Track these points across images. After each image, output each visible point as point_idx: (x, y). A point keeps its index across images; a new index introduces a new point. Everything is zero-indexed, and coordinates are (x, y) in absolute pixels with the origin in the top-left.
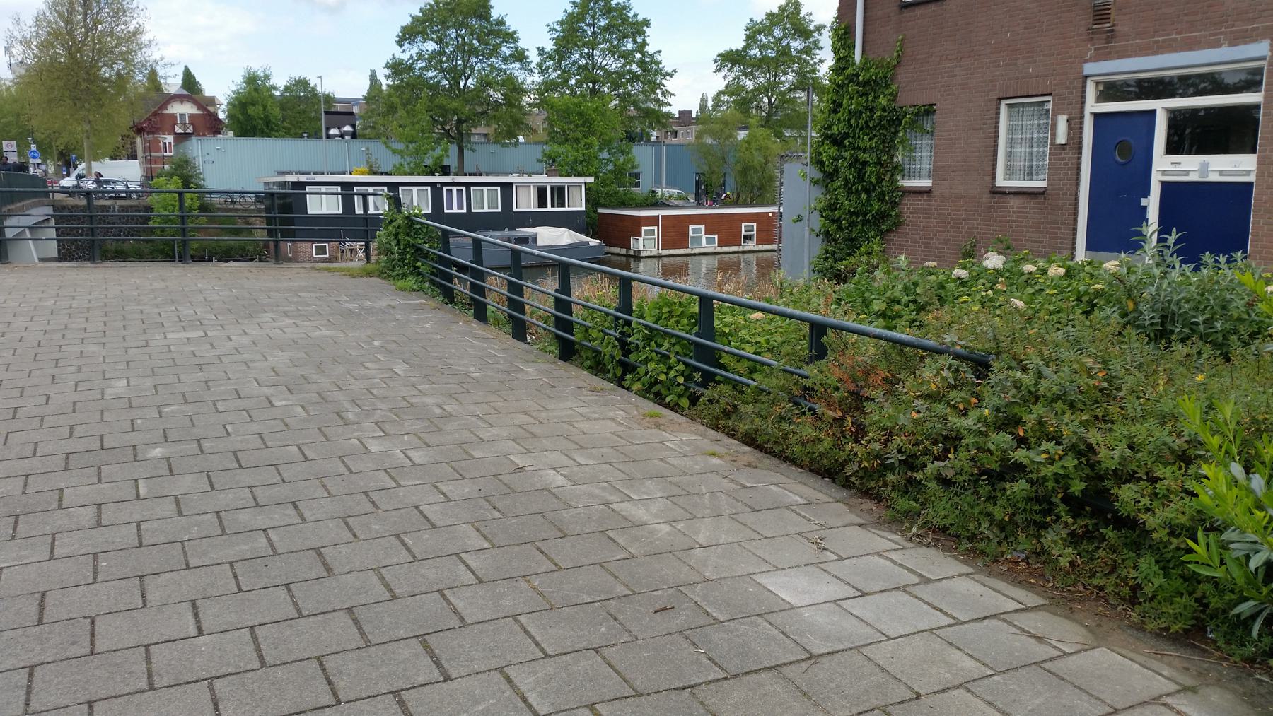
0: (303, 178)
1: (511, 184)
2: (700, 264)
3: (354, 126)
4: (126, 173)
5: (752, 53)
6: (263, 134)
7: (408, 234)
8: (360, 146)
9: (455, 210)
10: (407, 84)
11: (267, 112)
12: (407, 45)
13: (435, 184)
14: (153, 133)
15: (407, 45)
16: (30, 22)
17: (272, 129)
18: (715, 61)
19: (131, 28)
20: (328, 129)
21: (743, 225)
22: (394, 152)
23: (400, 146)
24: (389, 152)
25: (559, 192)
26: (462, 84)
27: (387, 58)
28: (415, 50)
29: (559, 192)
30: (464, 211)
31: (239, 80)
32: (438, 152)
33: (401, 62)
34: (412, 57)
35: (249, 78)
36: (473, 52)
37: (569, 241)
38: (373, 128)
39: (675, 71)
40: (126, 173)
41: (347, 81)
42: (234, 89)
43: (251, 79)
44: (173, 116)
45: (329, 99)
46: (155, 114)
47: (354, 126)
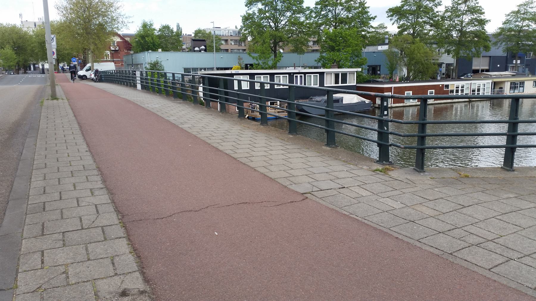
1: (323, 73)
2: (409, 111)
5: (405, 8)
18: (387, 12)
20: (194, 48)
21: (429, 91)
22: (253, 58)
24: (251, 58)
25: (344, 75)
29: (344, 75)
37: (357, 101)
39: (376, 17)
43: (145, 26)
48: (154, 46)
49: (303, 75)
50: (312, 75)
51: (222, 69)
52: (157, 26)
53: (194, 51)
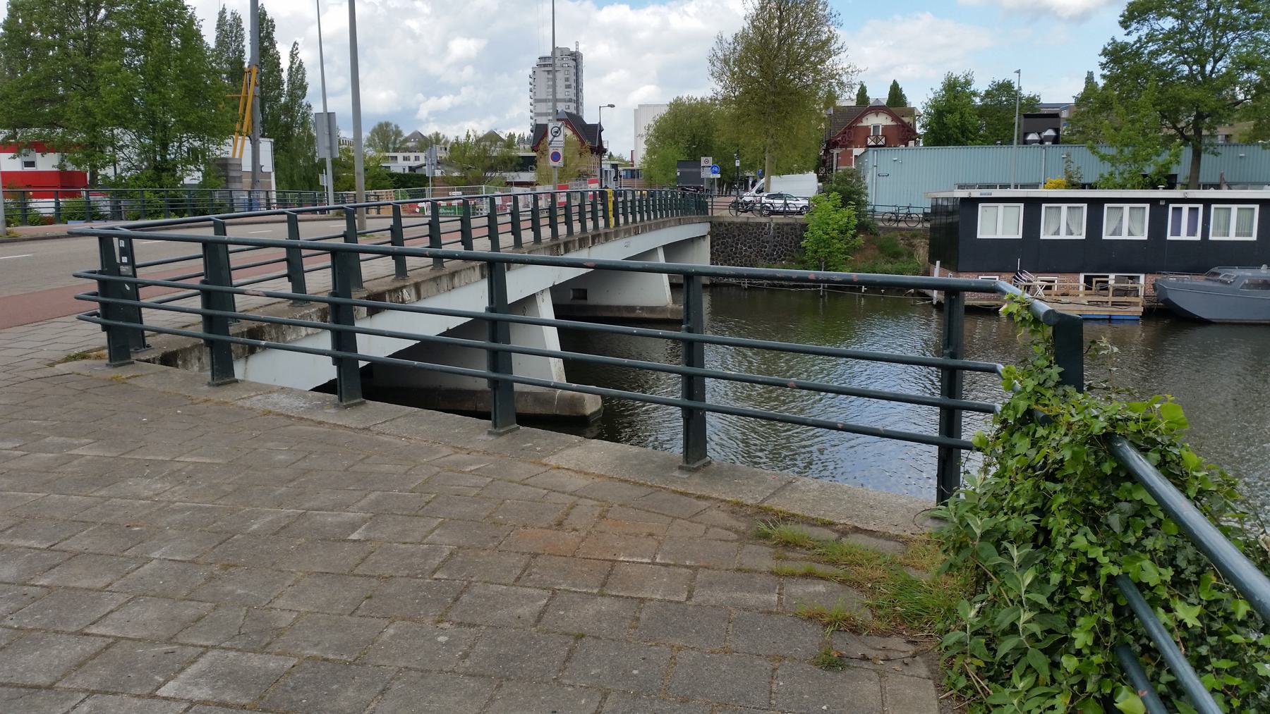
0: (976, 193)
3: (1057, 130)
4: (800, 188)
6: (958, 143)
7: (1092, 518)
8: (1060, 152)
9: (1184, 236)
10: (1130, 72)
11: (966, 119)
12: (1134, 25)
13: (1158, 200)
14: (846, 146)
15: (1134, 25)
16: (731, 40)
17: (968, 138)
19: (824, 37)
20: (1026, 134)
22: (1103, 158)
23: (1113, 151)
24: (1097, 159)
26: (1209, 68)
27: (1105, 41)
28: (1145, 30)
30: (1198, 237)
31: (938, 87)
32: (1166, 156)
33: (1125, 46)
34: (1140, 39)
35: (949, 85)
36: (1231, 25)
38: (1082, 133)
40: (800, 188)
41: (1058, 83)
42: (932, 96)
44: (867, 128)
45: (1033, 101)
46: (850, 127)
47: (1057, 130)
48: (963, 133)
49: (1201, 206)
50: (1234, 207)
51: (1023, 187)
52: (981, 85)
53: (1025, 142)
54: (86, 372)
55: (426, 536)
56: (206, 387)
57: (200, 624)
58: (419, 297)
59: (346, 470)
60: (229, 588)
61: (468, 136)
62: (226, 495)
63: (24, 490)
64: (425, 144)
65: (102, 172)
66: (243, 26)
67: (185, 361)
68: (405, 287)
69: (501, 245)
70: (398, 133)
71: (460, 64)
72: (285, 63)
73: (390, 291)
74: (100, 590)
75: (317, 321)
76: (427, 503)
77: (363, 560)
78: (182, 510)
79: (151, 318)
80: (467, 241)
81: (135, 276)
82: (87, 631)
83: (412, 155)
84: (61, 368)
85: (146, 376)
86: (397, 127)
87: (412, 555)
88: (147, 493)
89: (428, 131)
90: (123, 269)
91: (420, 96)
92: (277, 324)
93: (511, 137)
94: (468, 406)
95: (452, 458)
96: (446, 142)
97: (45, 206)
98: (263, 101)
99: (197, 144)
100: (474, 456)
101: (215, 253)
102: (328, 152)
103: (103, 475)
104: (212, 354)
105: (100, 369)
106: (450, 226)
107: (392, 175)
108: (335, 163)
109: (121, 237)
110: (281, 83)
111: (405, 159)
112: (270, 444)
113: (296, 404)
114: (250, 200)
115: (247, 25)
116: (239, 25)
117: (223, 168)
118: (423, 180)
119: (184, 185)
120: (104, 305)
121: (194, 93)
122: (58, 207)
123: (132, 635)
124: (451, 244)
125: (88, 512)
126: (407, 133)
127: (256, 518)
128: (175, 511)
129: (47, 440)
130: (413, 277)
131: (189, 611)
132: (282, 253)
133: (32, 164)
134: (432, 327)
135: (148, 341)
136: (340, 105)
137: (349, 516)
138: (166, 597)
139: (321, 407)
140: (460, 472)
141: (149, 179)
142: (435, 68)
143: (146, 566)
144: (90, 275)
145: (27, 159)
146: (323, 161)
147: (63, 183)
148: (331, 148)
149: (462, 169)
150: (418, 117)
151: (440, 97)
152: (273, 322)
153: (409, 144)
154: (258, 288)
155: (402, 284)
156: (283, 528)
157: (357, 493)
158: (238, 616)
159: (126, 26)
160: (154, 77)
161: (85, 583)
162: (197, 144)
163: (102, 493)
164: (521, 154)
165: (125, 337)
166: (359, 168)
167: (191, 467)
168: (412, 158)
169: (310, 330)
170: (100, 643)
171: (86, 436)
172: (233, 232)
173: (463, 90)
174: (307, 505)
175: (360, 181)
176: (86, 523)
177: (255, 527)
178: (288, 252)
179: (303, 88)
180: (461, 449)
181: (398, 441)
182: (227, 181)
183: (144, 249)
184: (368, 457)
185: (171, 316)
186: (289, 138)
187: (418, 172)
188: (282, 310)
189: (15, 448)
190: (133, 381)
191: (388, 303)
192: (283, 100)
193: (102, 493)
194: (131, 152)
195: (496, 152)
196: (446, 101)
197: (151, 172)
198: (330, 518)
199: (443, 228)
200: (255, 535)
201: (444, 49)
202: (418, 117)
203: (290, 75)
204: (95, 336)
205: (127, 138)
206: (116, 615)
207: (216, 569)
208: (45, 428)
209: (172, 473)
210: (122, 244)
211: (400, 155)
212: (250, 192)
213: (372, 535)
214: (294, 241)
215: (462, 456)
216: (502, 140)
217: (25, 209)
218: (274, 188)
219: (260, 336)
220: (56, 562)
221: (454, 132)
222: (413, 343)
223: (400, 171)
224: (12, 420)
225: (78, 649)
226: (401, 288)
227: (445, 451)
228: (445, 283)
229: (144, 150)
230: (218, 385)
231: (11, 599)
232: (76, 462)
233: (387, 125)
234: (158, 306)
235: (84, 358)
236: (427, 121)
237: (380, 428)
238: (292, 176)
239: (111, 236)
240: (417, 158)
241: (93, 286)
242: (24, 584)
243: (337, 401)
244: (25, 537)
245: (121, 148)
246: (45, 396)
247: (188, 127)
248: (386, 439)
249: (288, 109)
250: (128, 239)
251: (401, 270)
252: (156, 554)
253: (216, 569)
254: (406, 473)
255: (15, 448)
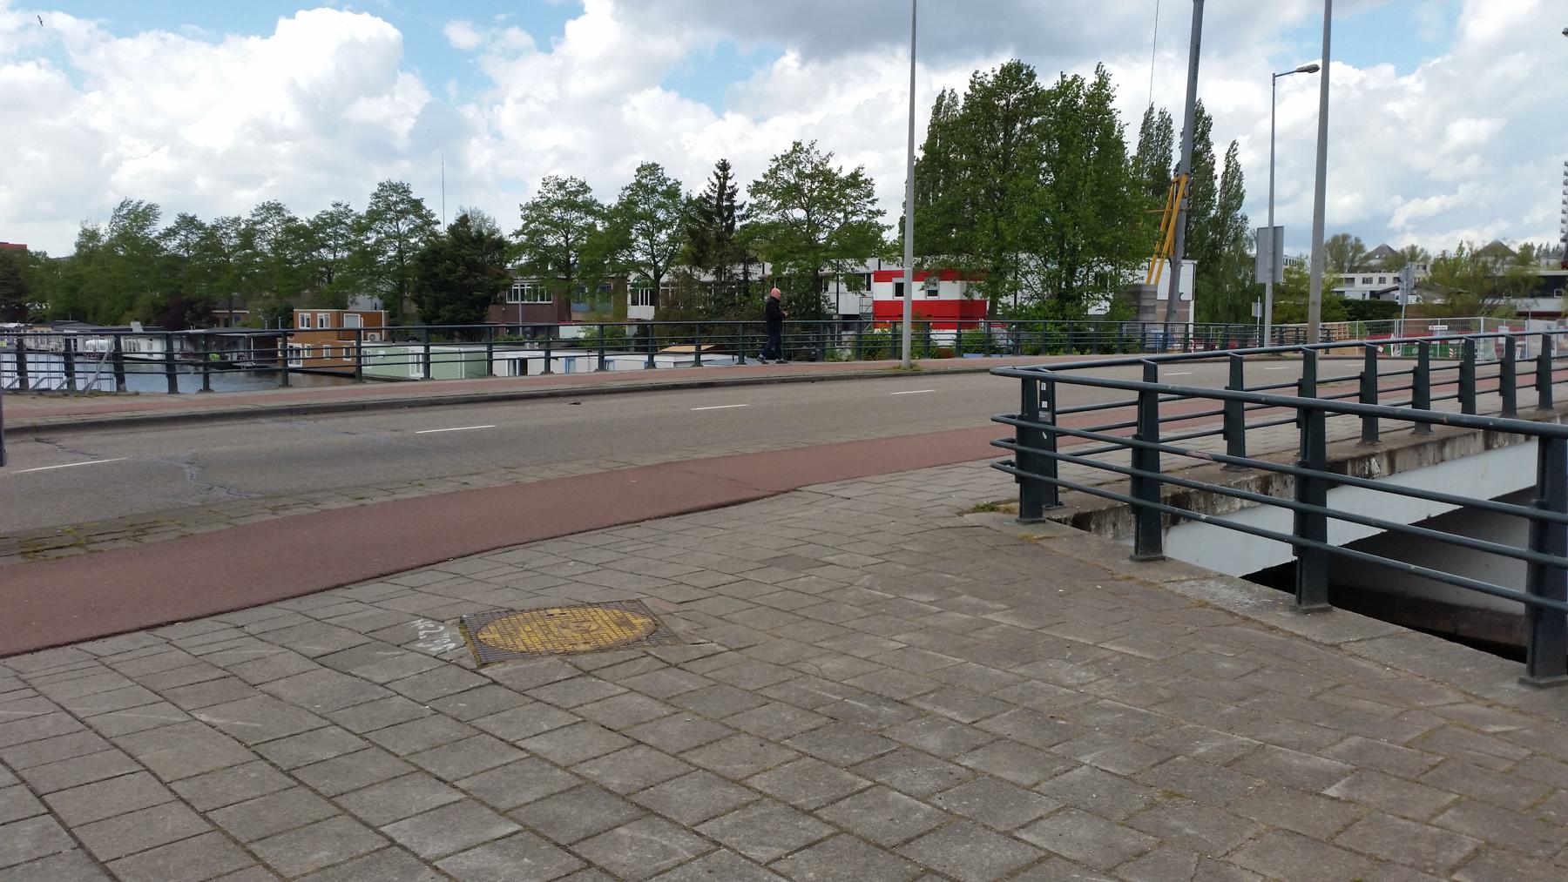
54: (996, 527)
55: (1434, 816)
56: (1127, 562)
57: (1143, 861)
58: (1392, 470)
59: (1312, 698)
60: (1174, 823)
61: (1461, 249)
62: (1162, 701)
63: (941, 652)
64: (1396, 261)
65: (1004, 300)
66: (1173, 127)
67: (1099, 526)
68: (1373, 455)
69: (1519, 403)
70: (1358, 248)
71: (1461, 154)
72: (1219, 169)
73: (1353, 460)
74: (1028, 788)
75: (1255, 492)
76: (1434, 767)
77: (1346, 827)
78: (1112, 710)
79: (1067, 472)
80: (1466, 396)
81: (1054, 423)
82: (1017, 834)
83: (1376, 276)
84: (970, 518)
85: (1061, 540)
86: (1357, 240)
87: (1416, 837)
88: (1069, 681)
89: (1400, 245)
90: (1042, 415)
91: (1398, 199)
92: (1208, 492)
93: (1527, 249)
94: (1444, 625)
95: (1465, 708)
96: (1426, 258)
97: (944, 337)
98: (1190, 214)
99: (1108, 268)
100: (1495, 712)
101: (1148, 399)
102: (1269, 275)
103: (1020, 650)
104: (1138, 523)
105: (1008, 524)
106: (1444, 371)
107: (1347, 303)
108: (1279, 291)
109: (1043, 379)
110: (1212, 191)
111: (1365, 281)
112: (1210, 646)
113: (1240, 597)
114: (1165, 334)
115: (1178, 125)
116: (1168, 127)
117: (1135, 297)
118: (1392, 309)
119: (1088, 317)
120: (1020, 454)
121: (1110, 209)
122: (958, 341)
123: (1066, 854)
124: (1445, 404)
125: (1008, 690)
126: (1370, 248)
127: (1202, 740)
128: (1103, 710)
129: (962, 598)
130: (1386, 442)
131: (1130, 841)
132: (1134, 396)
133: (935, 293)
134: (1405, 513)
135: (1061, 497)
136: (1295, 215)
137: (1321, 762)
138: (1100, 815)
139: (1273, 606)
140: (1477, 731)
141: (1052, 309)
142: (1421, 161)
143: (1076, 771)
144: (1008, 420)
145: (932, 288)
146: (1263, 286)
147: (963, 313)
148: (1274, 271)
149: (1449, 295)
150: (1390, 225)
151: (1425, 198)
152: (1201, 489)
153: (1373, 262)
154: (1192, 443)
155: (1370, 450)
156: (1237, 759)
157: (1331, 733)
158: (1189, 863)
159: (1045, 137)
160: (1065, 194)
161: (1010, 775)
162: (1108, 268)
163: (1021, 670)
164: (1544, 272)
165: (1037, 493)
166: (1315, 297)
167: (1118, 658)
168: (1376, 281)
169: (1246, 503)
170: (1031, 854)
171: (1000, 600)
172: (1169, 375)
173: (1462, 188)
174: (1265, 736)
175: (1315, 312)
176: (1007, 704)
177: (1201, 750)
178: (1141, 395)
179: (1239, 197)
180: (1477, 697)
181: (1380, 670)
182: (1138, 312)
183: (1065, 396)
184: (1339, 685)
185: (1092, 469)
186: (1216, 258)
187: (1384, 298)
188: (1214, 476)
189: (931, 603)
190: (1044, 543)
191: (1349, 477)
192: (1213, 212)
193: (1021, 670)
194: (1035, 281)
195: (1502, 270)
196: (1434, 203)
197: (1053, 302)
198: (1297, 760)
199: (1434, 377)
200: (1200, 760)
201: (1440, 135)
202: (1390, 225)
203: (1224, 183)
204: (1009, 488)
205: (1032, 263)
206: (1046, 823)
207: (1157, 794)
208: (958, 584)
209: (1096, 661)
210: (1044, 388)
211: (1358, 277)
212: (1166, 325)
213: (1356, 796)
214: (1151, 385)
215: (1477, 709)
216: (1513, 253)
217: (927, 340)
218: (1191, 320)
219: (1188, 503)
220: (978, 743)
221: (1437, 245)
222: (1378, 531)
223: (1358, 296)
224: (926, 571)
225: (1009, 853)
226: (1369, 457)
227: (1452, 696)
228: (1431, 452)
229: (1049, 281)
230: (1142, 560)
231: (939, 774)
232: (991, 629)
233: (1345, 237)
234: (1073, 459)
235: (992, 510)
236: (1403, 231)
237: (1355, 648)
238: (1214, 305)
239: (1035, 378)
240: (1382, 280)
241: (1011, 432)
242: (949, 761)
243: (1294, 603)
244: (947, 706)
245: (1024, 275)
246: (956, 548)
247: (1100, 250)
248: (1365, 664)
249: (1218, 224)
250: (1051, 382)
251: (1370, 433)
252: (1087, 759)
253: (1157, 794)
254: (1396, 717)
255: (931, 603)
